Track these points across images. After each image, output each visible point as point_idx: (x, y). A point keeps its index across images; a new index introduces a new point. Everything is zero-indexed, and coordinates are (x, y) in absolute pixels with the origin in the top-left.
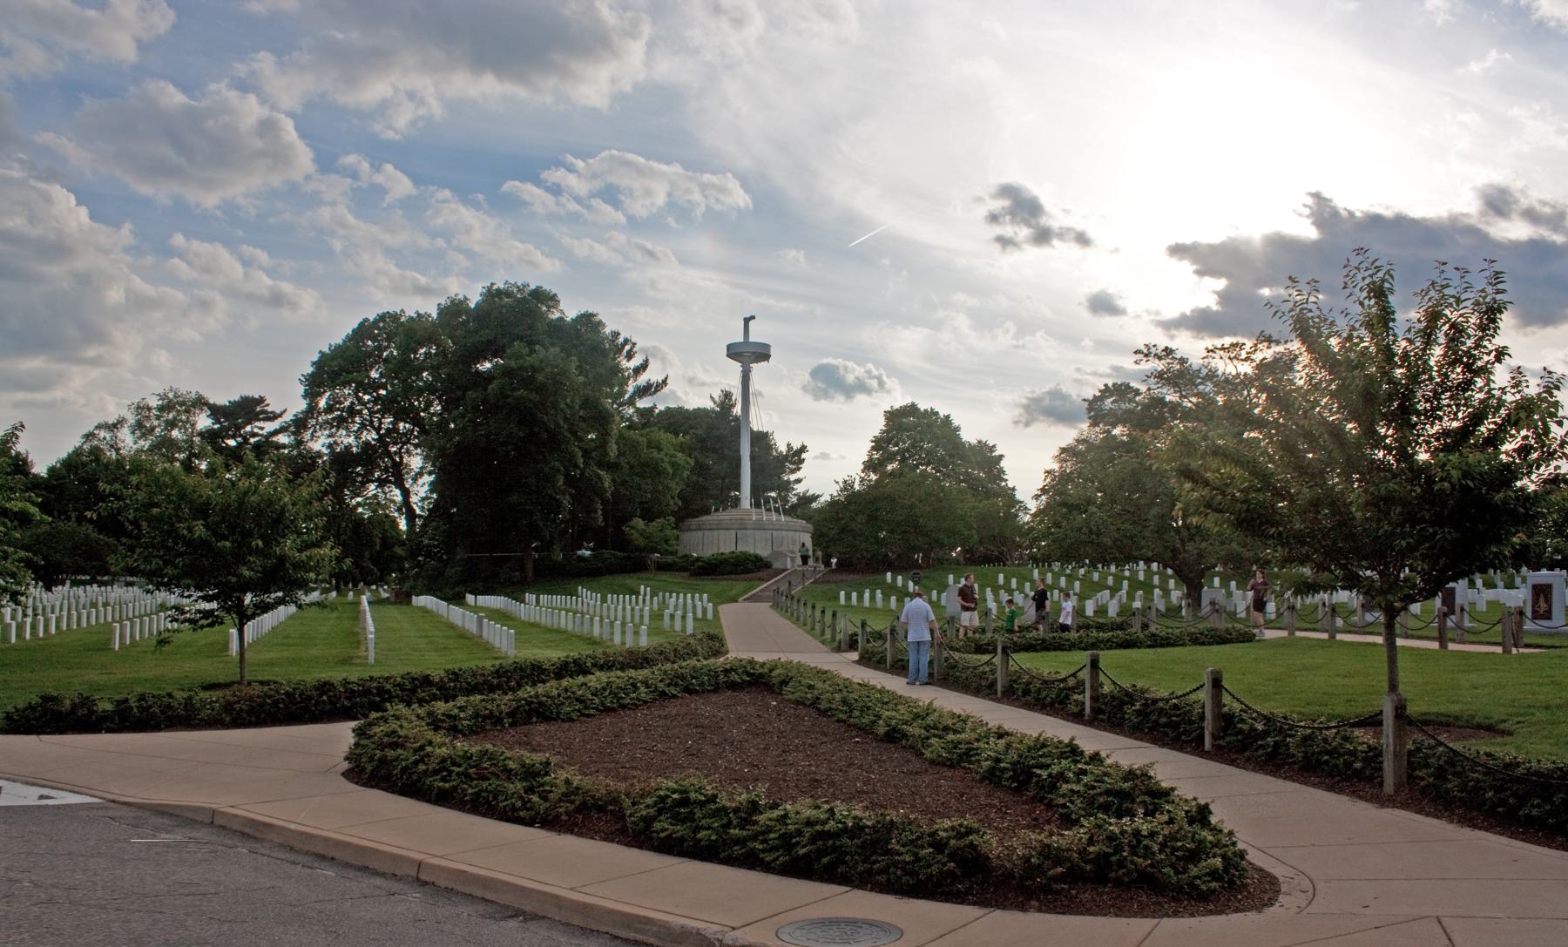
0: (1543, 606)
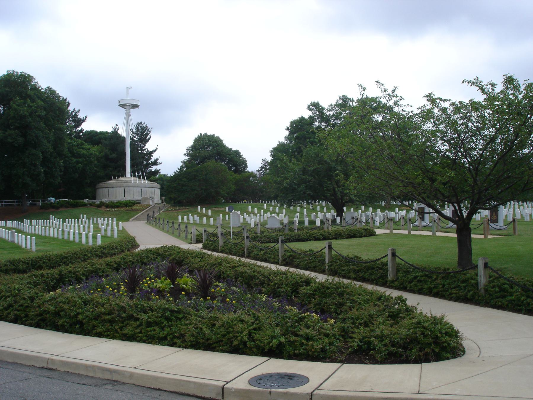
0: (495, 217)
